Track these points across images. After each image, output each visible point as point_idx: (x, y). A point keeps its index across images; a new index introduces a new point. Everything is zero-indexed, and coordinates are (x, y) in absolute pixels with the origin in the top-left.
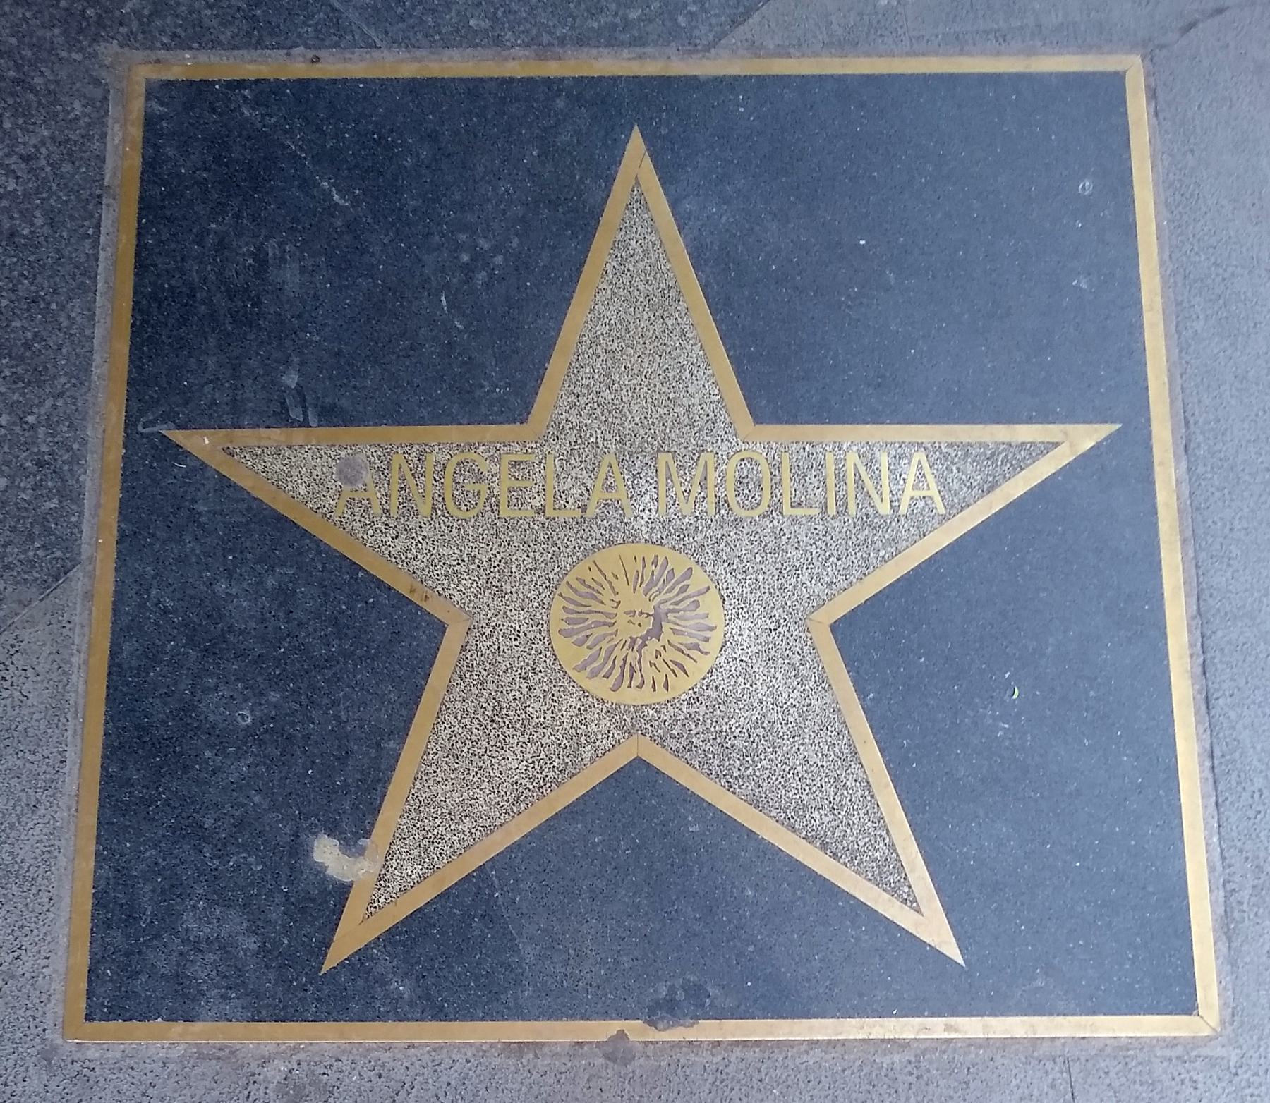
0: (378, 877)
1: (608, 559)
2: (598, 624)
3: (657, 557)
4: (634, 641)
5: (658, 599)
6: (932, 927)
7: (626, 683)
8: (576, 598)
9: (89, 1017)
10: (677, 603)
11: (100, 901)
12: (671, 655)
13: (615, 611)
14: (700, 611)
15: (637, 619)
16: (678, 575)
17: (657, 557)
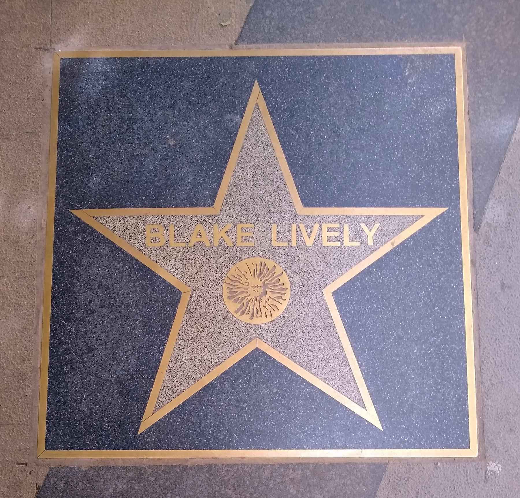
1: (243, 265)
2: (242, 293)
4: (256, 298)
5: (265, 279)
6: (370, 414)
9: (46, 449)
10: (271, 280)
12: (271, 302)
13: (247, 287)
14: (280, 283)
15: (256, 289)
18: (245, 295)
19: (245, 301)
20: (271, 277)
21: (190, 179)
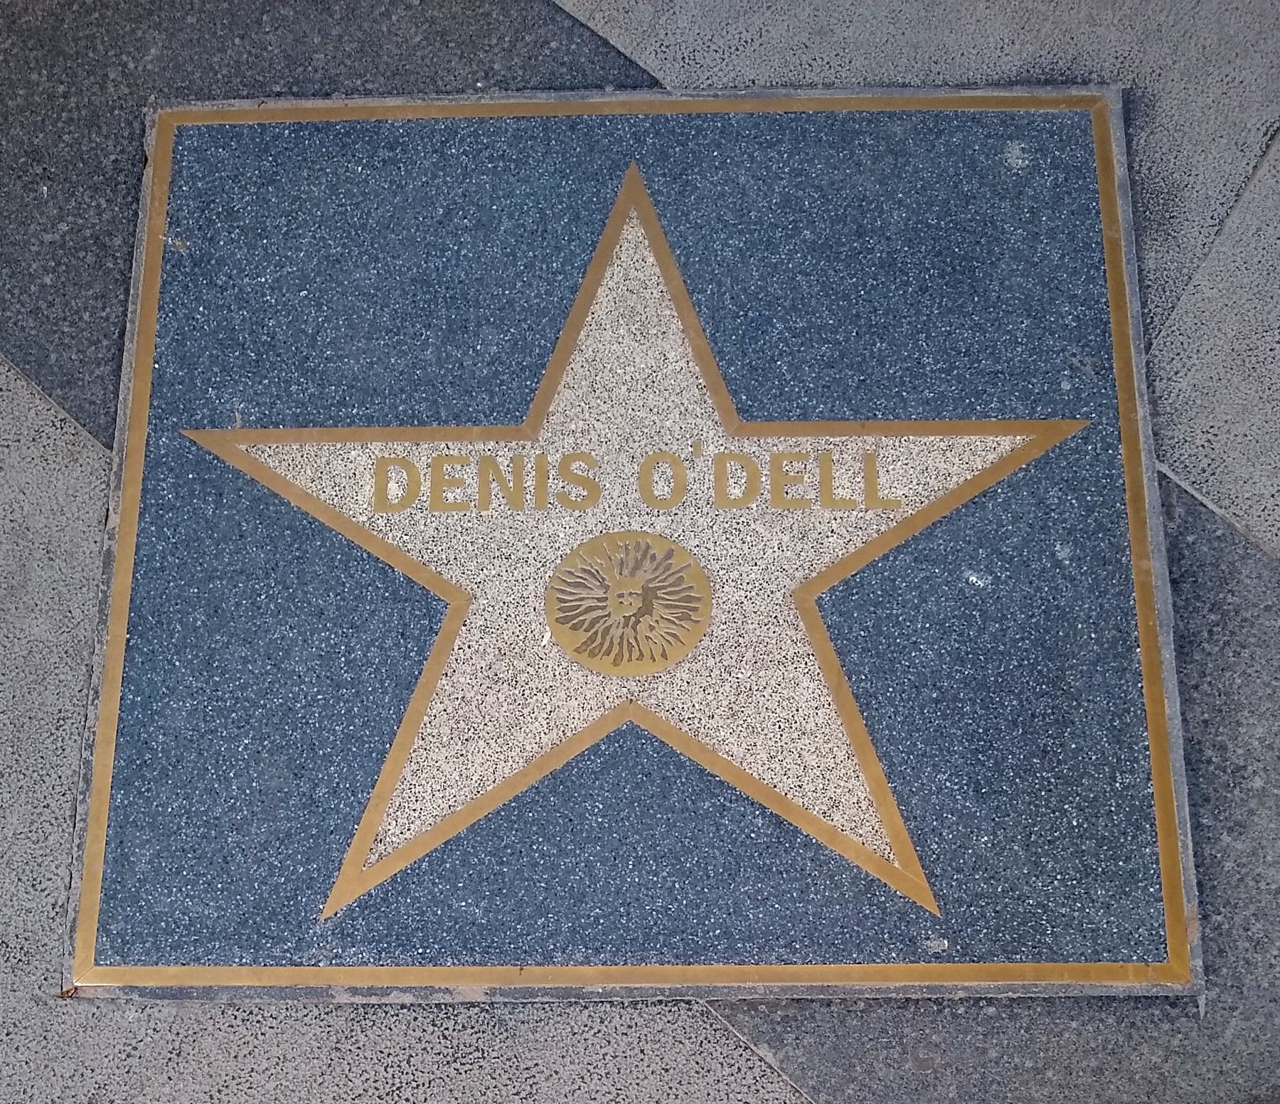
0: (348, 888)
18: (600, 613)
19: (600, 627)
21: (778, 364)
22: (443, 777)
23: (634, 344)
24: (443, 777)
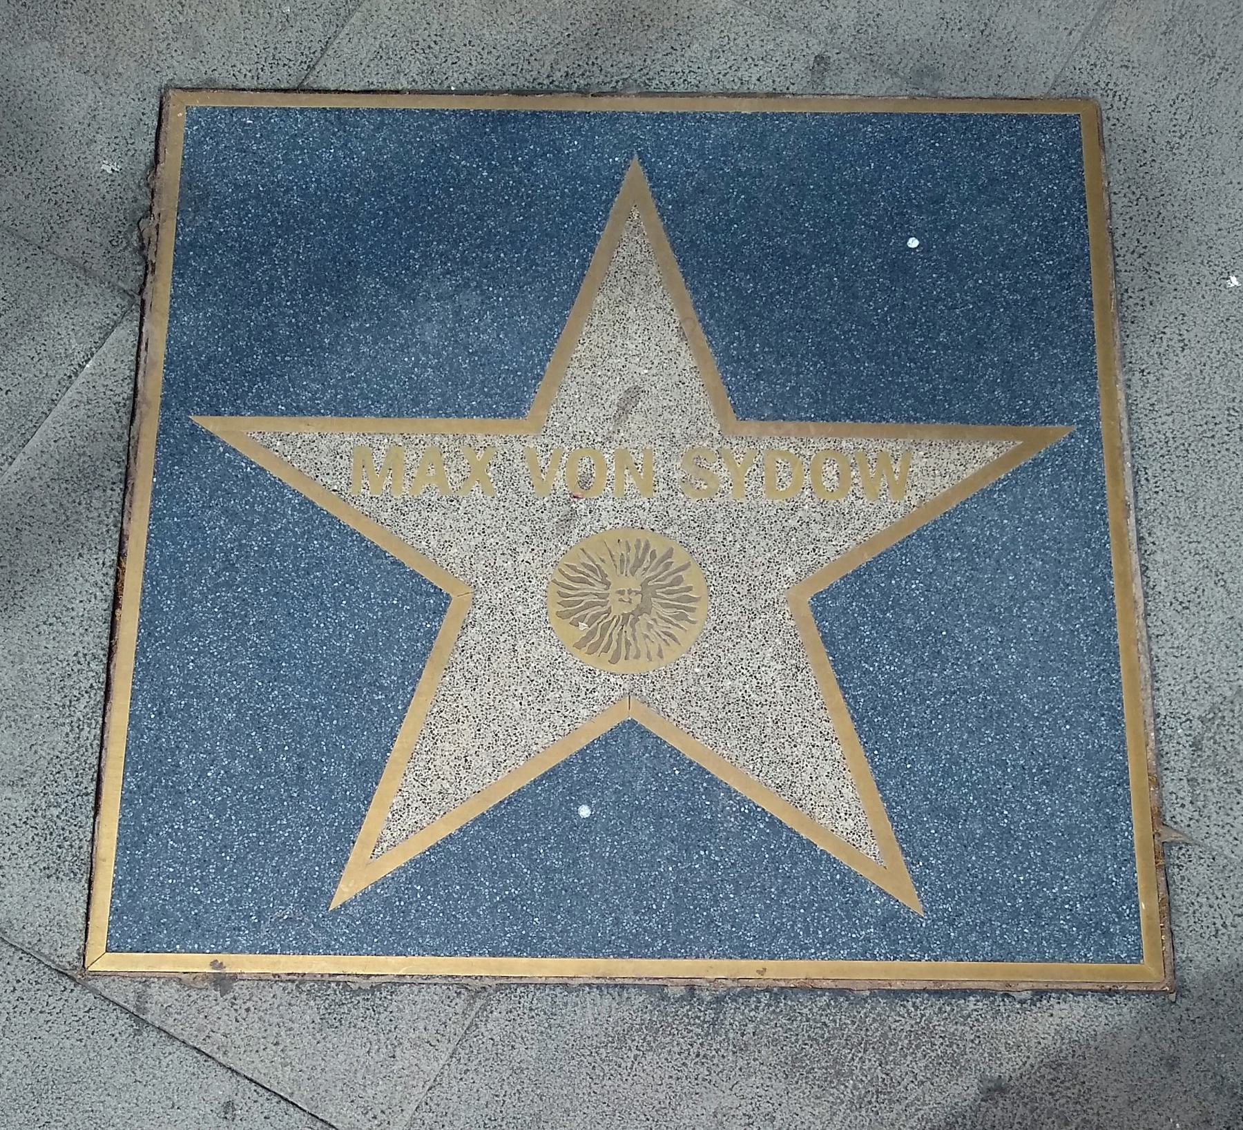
0: (389, 840)
2: (590, 605)
3: (639, 541)
7: (623, 653)
8: (567, 582)
11: (378, 775)
16: (659, 556)
17: (639, 541)
20: (661, 573)
22: (450, 762)
23: (636, 341)
24: (450, 762)
